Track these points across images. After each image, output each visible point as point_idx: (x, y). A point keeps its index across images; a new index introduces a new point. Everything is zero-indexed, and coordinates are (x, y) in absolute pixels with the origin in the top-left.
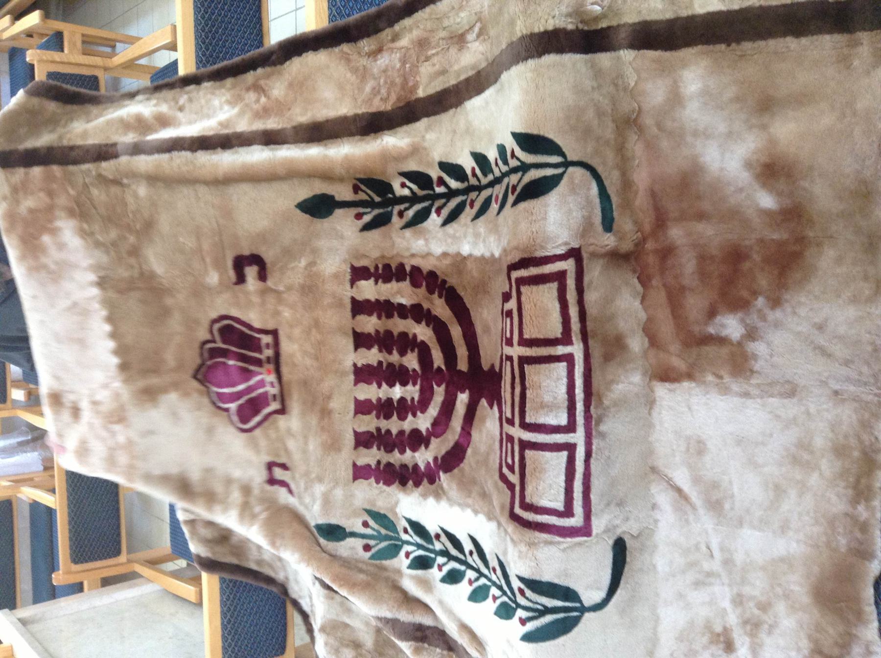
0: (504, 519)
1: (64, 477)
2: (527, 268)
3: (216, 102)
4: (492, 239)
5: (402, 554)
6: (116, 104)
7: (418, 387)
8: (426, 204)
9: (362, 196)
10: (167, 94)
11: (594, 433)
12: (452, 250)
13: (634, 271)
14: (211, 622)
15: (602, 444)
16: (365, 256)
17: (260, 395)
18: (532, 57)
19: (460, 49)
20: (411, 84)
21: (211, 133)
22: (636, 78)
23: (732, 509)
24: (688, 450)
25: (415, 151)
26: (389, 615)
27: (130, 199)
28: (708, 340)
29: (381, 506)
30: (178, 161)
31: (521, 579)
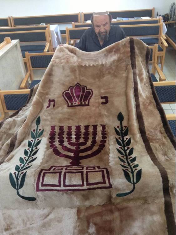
0: (41, 168)
1: (52, 54)
2: (107, 173)
3: (146, 93)
4: (114, 163)
5: (32, 139)
6: (146, 68)
7: (75, 142)
8: (122, 145)
9: (124, 128)
10: (148, 81)
11: (63, 192)
12: (111, 151)
13: (106, 203)
14: (15, 92)
15: (61, 194)
16: (108, 128)
17: (72, 100)
18: (161, 174)
19: (163, 154)
20: (153, 141)
21: (139, 92)
22: (157, 202)
23: (43, 230)
24: (59, 218)
25: (136, 142)
26: (18, 138)
27: (122, 72)
28: (88, 223)
29: (45, 133)
30: (132, 84)
31: (26, 173)
